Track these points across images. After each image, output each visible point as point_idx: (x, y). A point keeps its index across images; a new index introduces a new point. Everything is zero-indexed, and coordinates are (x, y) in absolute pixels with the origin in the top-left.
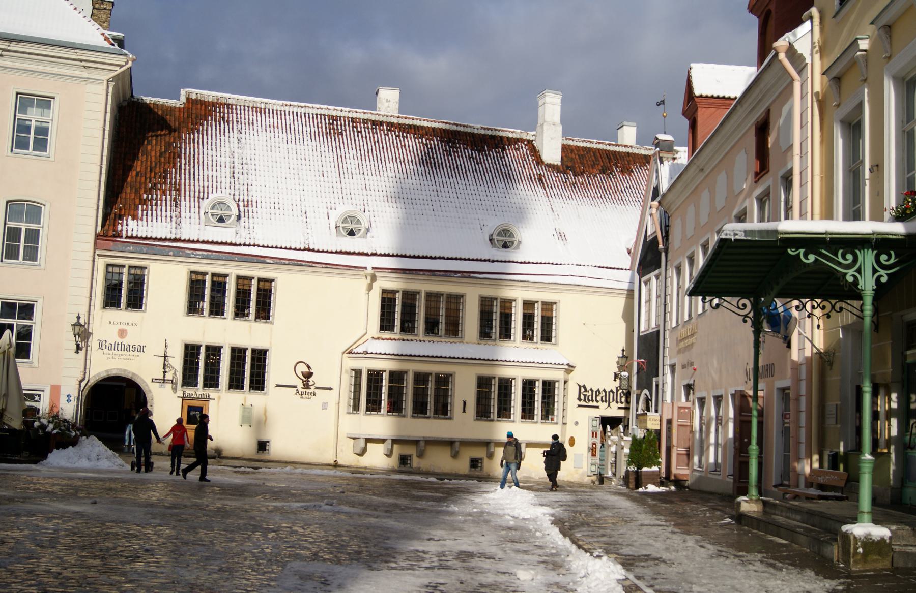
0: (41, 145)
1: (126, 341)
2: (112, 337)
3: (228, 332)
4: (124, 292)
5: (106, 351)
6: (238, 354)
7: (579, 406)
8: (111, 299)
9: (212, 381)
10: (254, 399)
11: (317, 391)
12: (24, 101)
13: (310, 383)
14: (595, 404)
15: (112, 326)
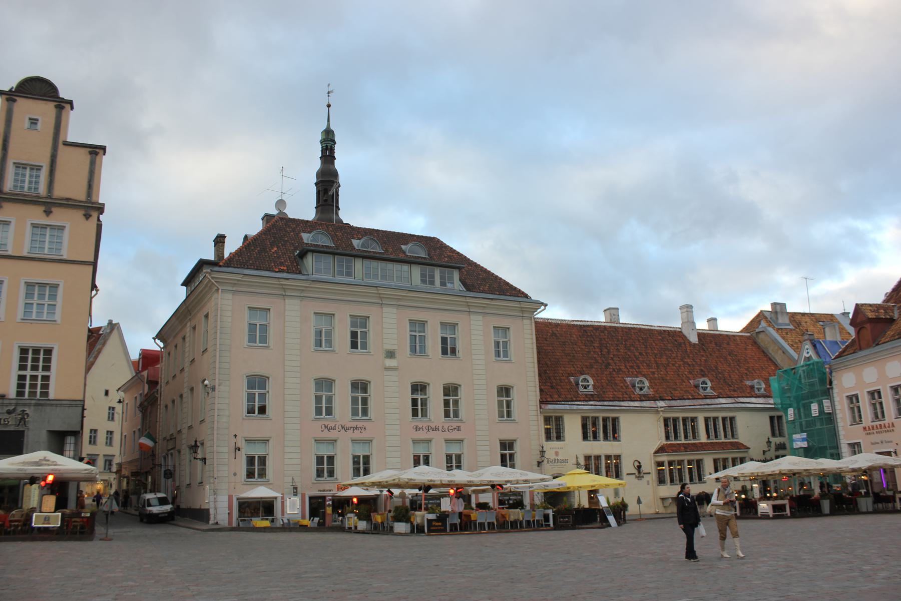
1: (559, 458)
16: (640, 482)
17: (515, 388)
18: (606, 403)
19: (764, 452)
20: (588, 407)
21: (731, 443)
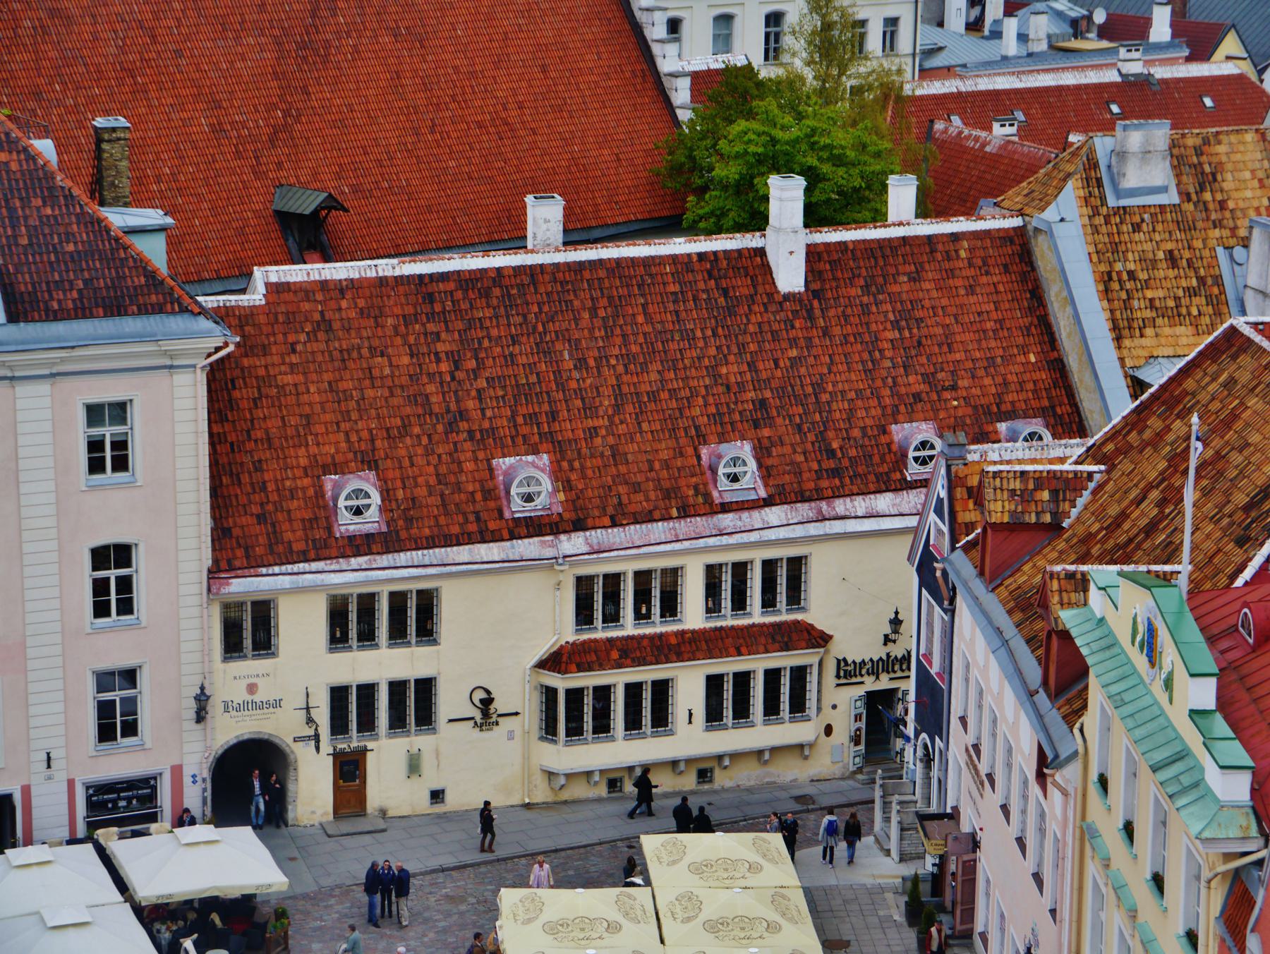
0: (121, 464)
1: (257, 698)
2: (240, 695)
3: (383, 664)
4: (249, 631)
5: (234, 713)
6: (397, 688)
7: (838, 685)
8: (232, 647)
9: (367, 723)
10: (420, 741)
11: (500, 720)
12: (94, 413)
13: (492, 711)
14: (859, 679)
15: (238, 681)
16: (486, 735)
17: (141, 548)
18: (403, 558)
19: (887, 640)
20: (349, 576)
21: (723, 653)
